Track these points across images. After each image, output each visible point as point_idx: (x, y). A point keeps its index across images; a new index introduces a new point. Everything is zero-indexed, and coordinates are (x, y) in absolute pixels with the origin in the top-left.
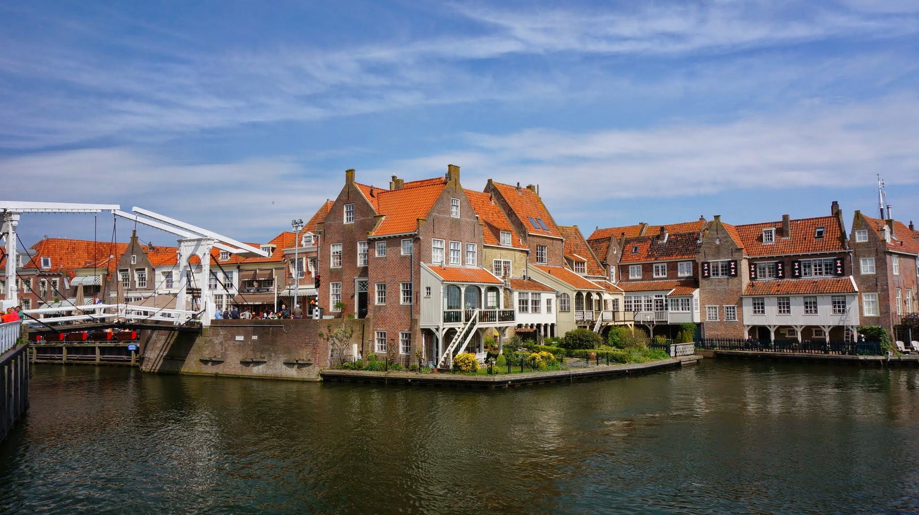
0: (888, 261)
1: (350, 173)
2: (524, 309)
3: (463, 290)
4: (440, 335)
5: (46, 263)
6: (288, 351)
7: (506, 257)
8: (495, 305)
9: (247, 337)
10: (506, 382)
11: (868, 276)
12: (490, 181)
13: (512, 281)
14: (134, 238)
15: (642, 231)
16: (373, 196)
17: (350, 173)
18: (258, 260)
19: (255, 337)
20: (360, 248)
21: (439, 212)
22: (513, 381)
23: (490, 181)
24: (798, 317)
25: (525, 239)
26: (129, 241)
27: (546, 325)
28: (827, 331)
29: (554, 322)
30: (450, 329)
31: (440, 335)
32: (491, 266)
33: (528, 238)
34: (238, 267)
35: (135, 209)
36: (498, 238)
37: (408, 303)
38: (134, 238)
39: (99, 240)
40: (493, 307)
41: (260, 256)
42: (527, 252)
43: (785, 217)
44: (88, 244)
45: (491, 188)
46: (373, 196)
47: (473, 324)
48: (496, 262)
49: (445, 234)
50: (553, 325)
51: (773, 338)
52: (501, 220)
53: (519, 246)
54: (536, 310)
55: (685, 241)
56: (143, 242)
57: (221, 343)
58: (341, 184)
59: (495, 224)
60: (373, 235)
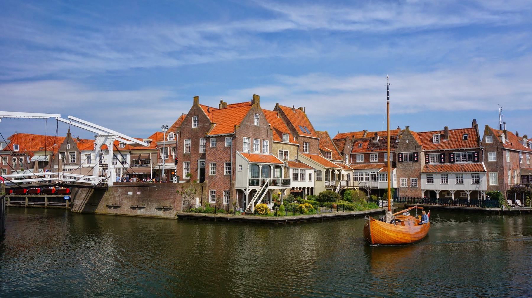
1: (196, 99)
2: (295, 179)
3: (261, 167)
4: (247, 193)
5: (16, 148)
6: (158, 201)
8: (279, 176)
10: (285, 221)
12: (277, 105)
13: (289, 162)
14: (69, 134)
15: (364, 134)
16: (209, 112)
17: (196, 99)
18: (141, 148)
19: (139, 193)
20: (201, 142)
21: (247, 122)
22: (288, 220)
23: (277, 105)
24: (452, 185)
27: (308, 188)
28: (469, 193)
29: (313, 186)
30: (253, 190)
31: (247, 193)
32: (277, 154)
33: (299, 138)
34: (130, 152)
36: (281, 137)
38: (69, 134)
39: (48, 135)
40: (278, 177)
41: (143, 146)
42: (298, 146)
43: (446, 128)
44: (42, 137)
45: (278, 108)
46: (209, 112)
47: (266, 187)
48: (280, 151)
49: (251, 135)
50: (312, 188)
51: (438, 197)
52: (283, 127)
57: (119, 196)
58: (191, 105)
59: (280, 129)
60: (209, 134)
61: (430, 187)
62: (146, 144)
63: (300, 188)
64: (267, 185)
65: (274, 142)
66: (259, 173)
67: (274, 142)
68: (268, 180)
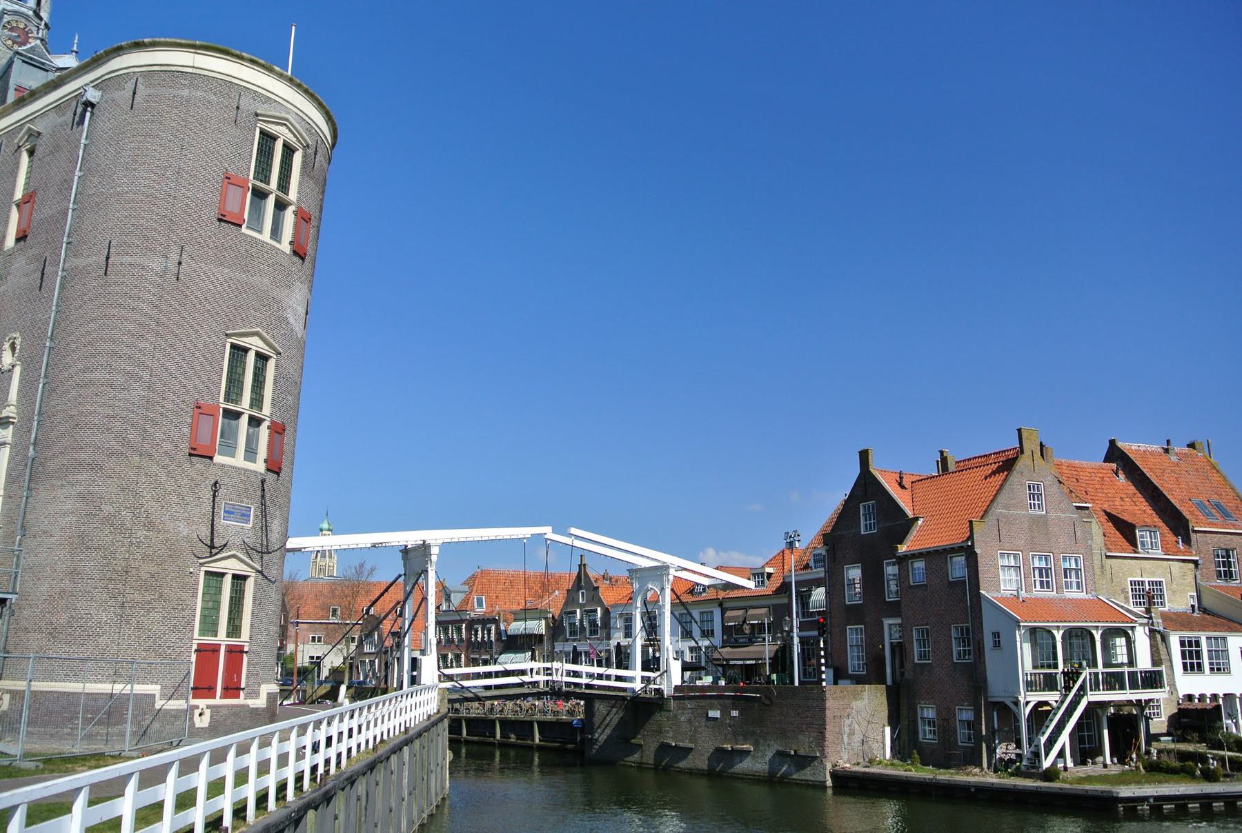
0: (831, 704)
1: (864, 456)
2: (1193, 665)
3: (1058, 636)
5: (480, 604)
6: (783, 735)
7: (1153, 574)
8: (1126, 661)
9: (725, 712)
10: (1144, 799)
11: (817, 725)
12: (1112, 443)
13: (1164, 616)
14: (582, 566)
16: (903, 487)
18: (746, 593)
19: (735, 713)
20: (891, 570)
21: (1007, 507)
22: (1157, 798)
23: (1112, 443)
25: (1187, 541)
26: (575, 571)
32: (1124, 591)
33: (1193, 536)
34: (721, 605)
35: (574, 531)
37: (968, 659)
38: (582, 566)
40: (1122, 665)
41: (743, 588)
42: (1195, 563)
46: (903, 487)
48: (1133, 583)
49: (1020, 542)
52: (1137, 509)
53: (1178, 552)
54: (1216, 669)
55: (50, 760)
56: (592, 573)
57: (689, 721)
58: (856, 472)
59: (1126, 517)
60: (902, 549)
61: (639, 680)
62: (750, 584)
63: (1202, 697)
64: (1082, 688)
65: (1107, 557)
66: (247, 677)
67: (1107, 557)
68: (1086, 673)
